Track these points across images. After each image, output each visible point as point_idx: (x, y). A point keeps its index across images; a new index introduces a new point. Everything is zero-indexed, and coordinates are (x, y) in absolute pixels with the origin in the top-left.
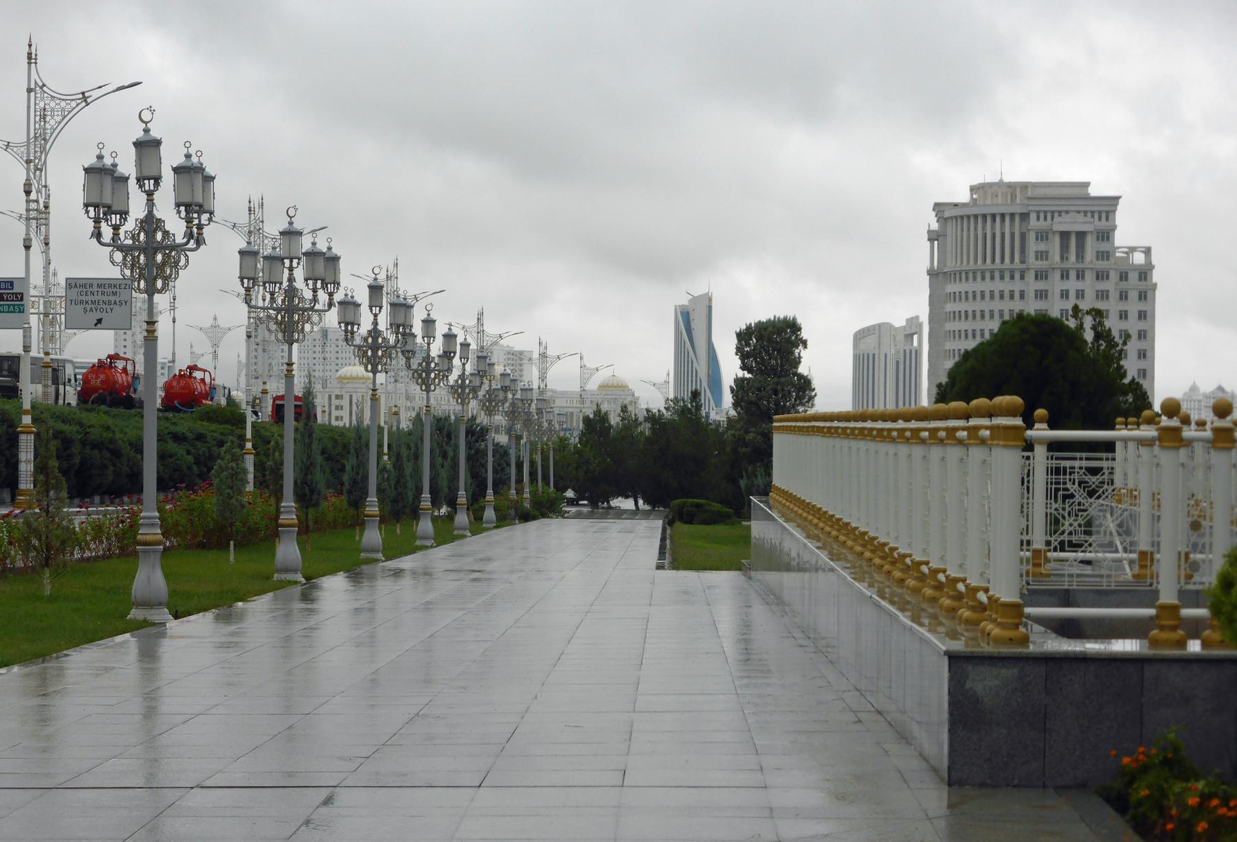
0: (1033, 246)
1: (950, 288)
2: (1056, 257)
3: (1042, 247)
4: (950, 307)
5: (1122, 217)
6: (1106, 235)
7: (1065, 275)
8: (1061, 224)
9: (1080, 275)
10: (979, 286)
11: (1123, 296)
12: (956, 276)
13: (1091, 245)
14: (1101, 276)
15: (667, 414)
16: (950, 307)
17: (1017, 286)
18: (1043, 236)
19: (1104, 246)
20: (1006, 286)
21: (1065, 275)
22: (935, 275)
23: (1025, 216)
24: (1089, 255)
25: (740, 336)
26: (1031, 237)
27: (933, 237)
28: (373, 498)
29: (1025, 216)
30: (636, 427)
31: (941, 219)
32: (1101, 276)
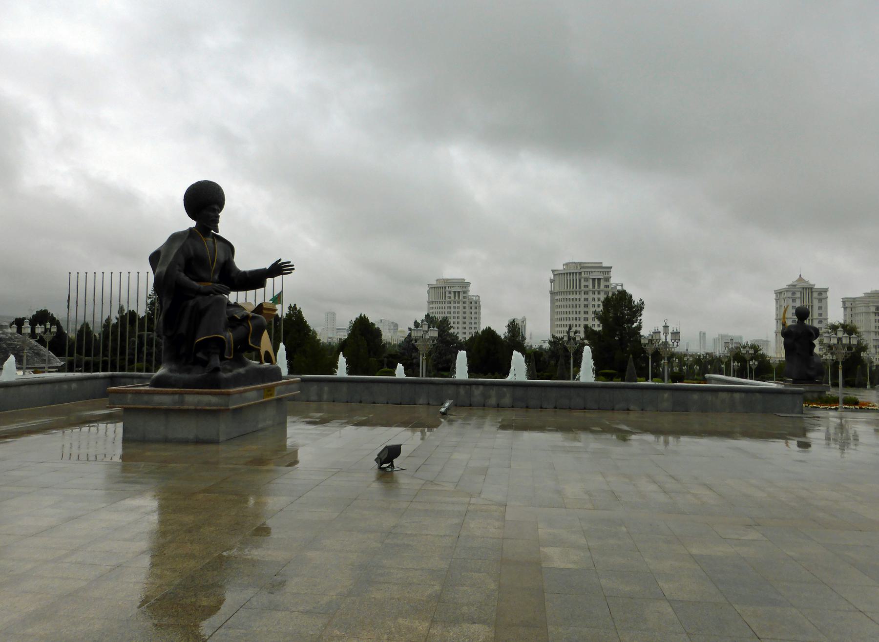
0: (583, 283)
1: (557, 297)
2: (591, 287)
3: (586, 283)
4: (557, 304)
5: (613, 273)
6: (465, 292)
7: (594, 293)
8: (453, 289)
9: (599, 293)
10: (439, 305)
11: (471, 308)
12: (559, 293)
13: (603, 284)
14: (464, 303)
15: (503, 337)
16: (557, 304)
17: (578, 296)
18: (586, 280)
19: (607, 284)
20: (575, 296)
21: (594, 293)
22: (552, 293)
23: (580, 273)
24: (602, 286)
25: (779, 293)
26: (582, 280)
27: (552, 281)
28: (235, 372)
29: (580, 273)
30: (594, 332)
31: (554, 275)
32: (464, 303)
